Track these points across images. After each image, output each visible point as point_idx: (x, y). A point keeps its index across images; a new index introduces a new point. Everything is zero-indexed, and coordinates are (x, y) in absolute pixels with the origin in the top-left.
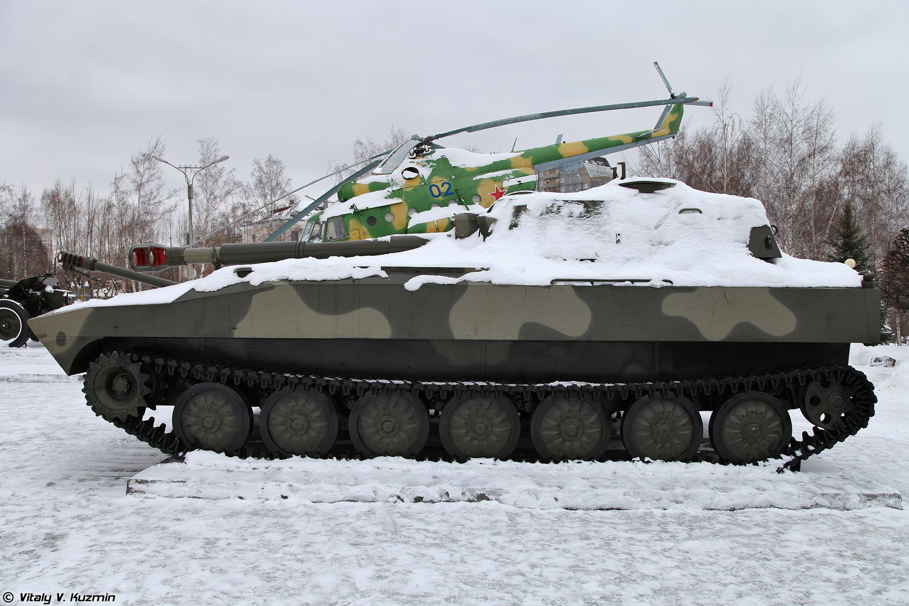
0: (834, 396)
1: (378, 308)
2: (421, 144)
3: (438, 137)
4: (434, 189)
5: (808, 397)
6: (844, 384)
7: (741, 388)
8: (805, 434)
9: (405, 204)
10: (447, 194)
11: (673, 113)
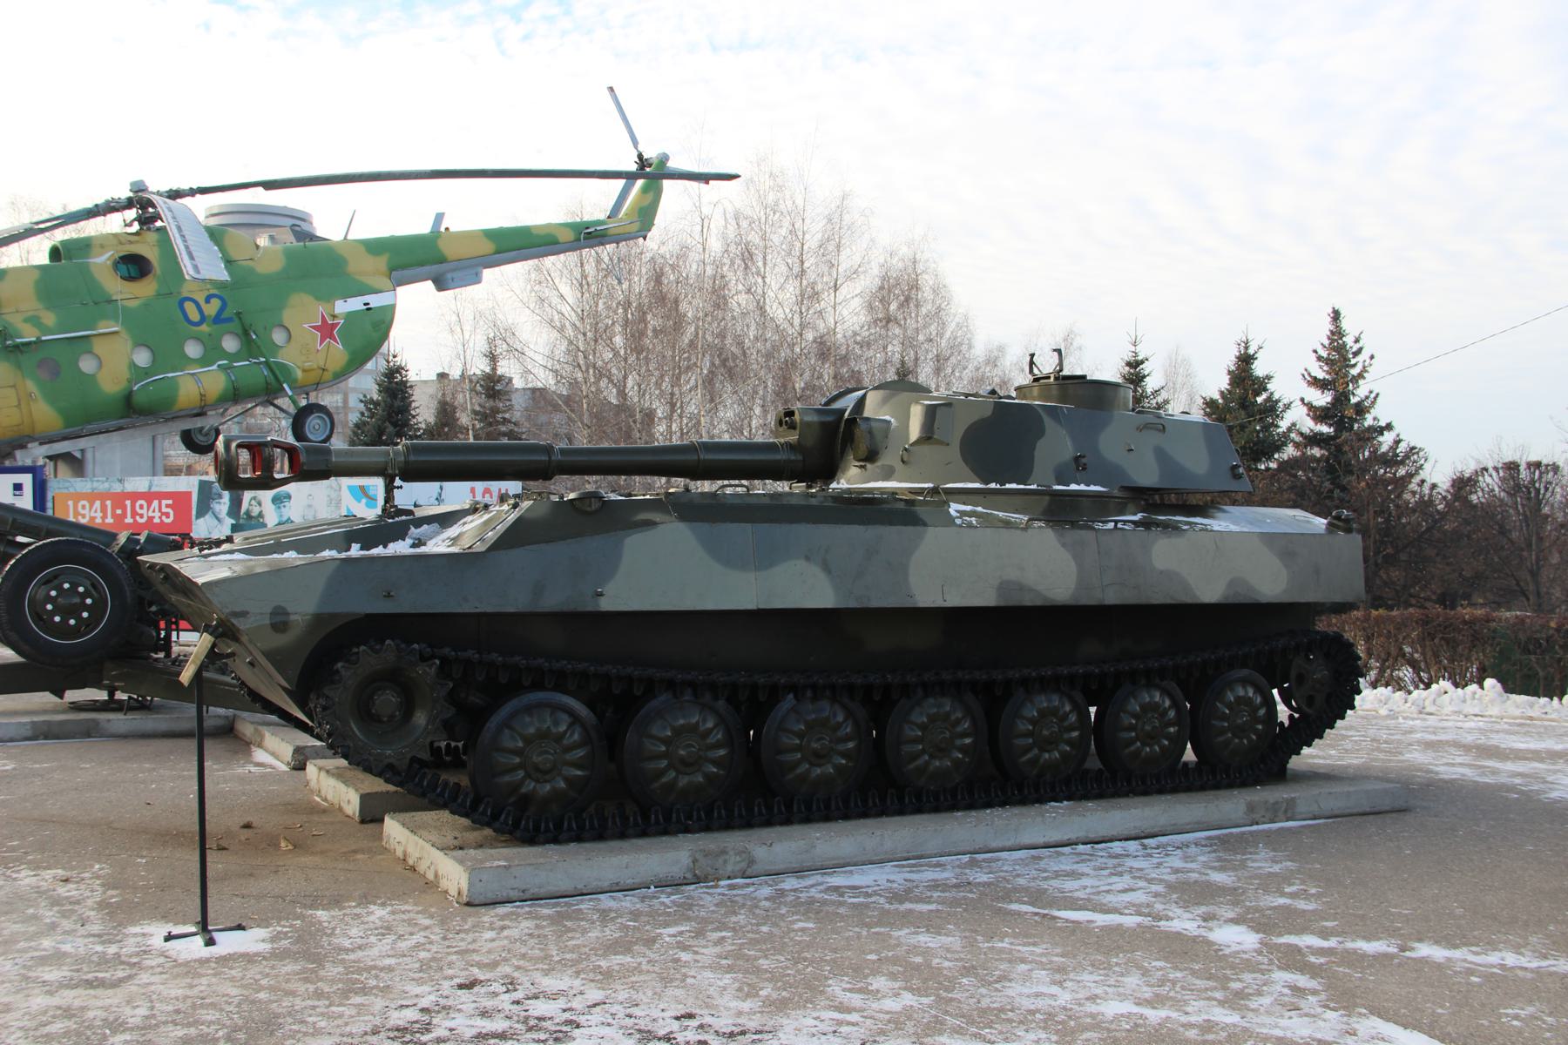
3: (193, 192)
4: (190, 308)
9: (124, 335)
10: (218, 319)
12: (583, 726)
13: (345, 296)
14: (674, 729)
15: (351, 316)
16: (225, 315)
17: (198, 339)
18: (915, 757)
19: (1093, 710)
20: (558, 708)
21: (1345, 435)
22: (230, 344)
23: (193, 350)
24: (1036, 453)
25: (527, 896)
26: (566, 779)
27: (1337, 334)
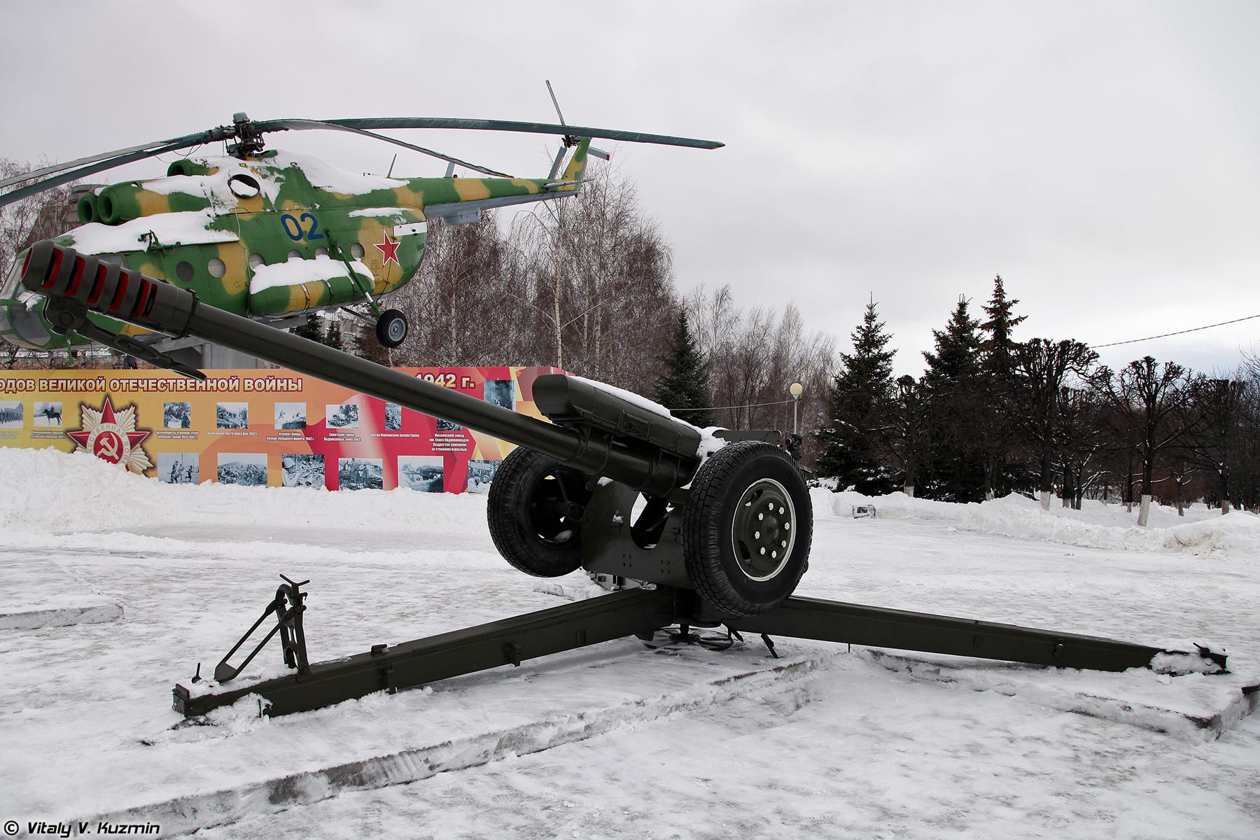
9: (243, 244)
10: (311, 235)
16: (317, 232)
21: (645, 297)
27: (999, 292)
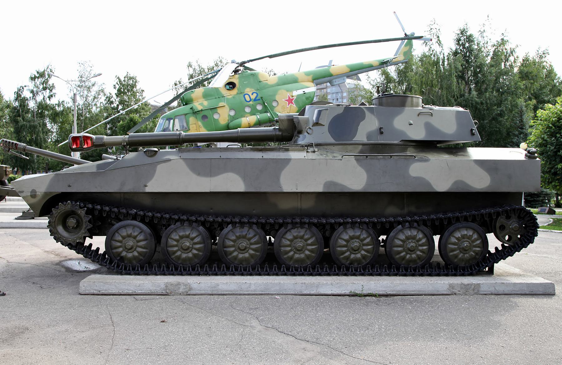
0: (513, 224)
1: (238, 173)
2: (238, 67)
3: (249, 61)
4: (247, 97)
5: (498, 225)
6: (519, 217)
7: (458, 219)
8: (496, 248)
9: (227, 106)
11: (406, 45)
12: (145, 233)
13: (297, 90)
14: (180, 236)
15: (298, 96)
17: (249, 106)
18: (343, 253)
19: (436, 238)
20: (134, 226)
22: (259, 107)
23: (248, 110)
24: (360, 128)
25: (100, 293)
26: (138, 252)
